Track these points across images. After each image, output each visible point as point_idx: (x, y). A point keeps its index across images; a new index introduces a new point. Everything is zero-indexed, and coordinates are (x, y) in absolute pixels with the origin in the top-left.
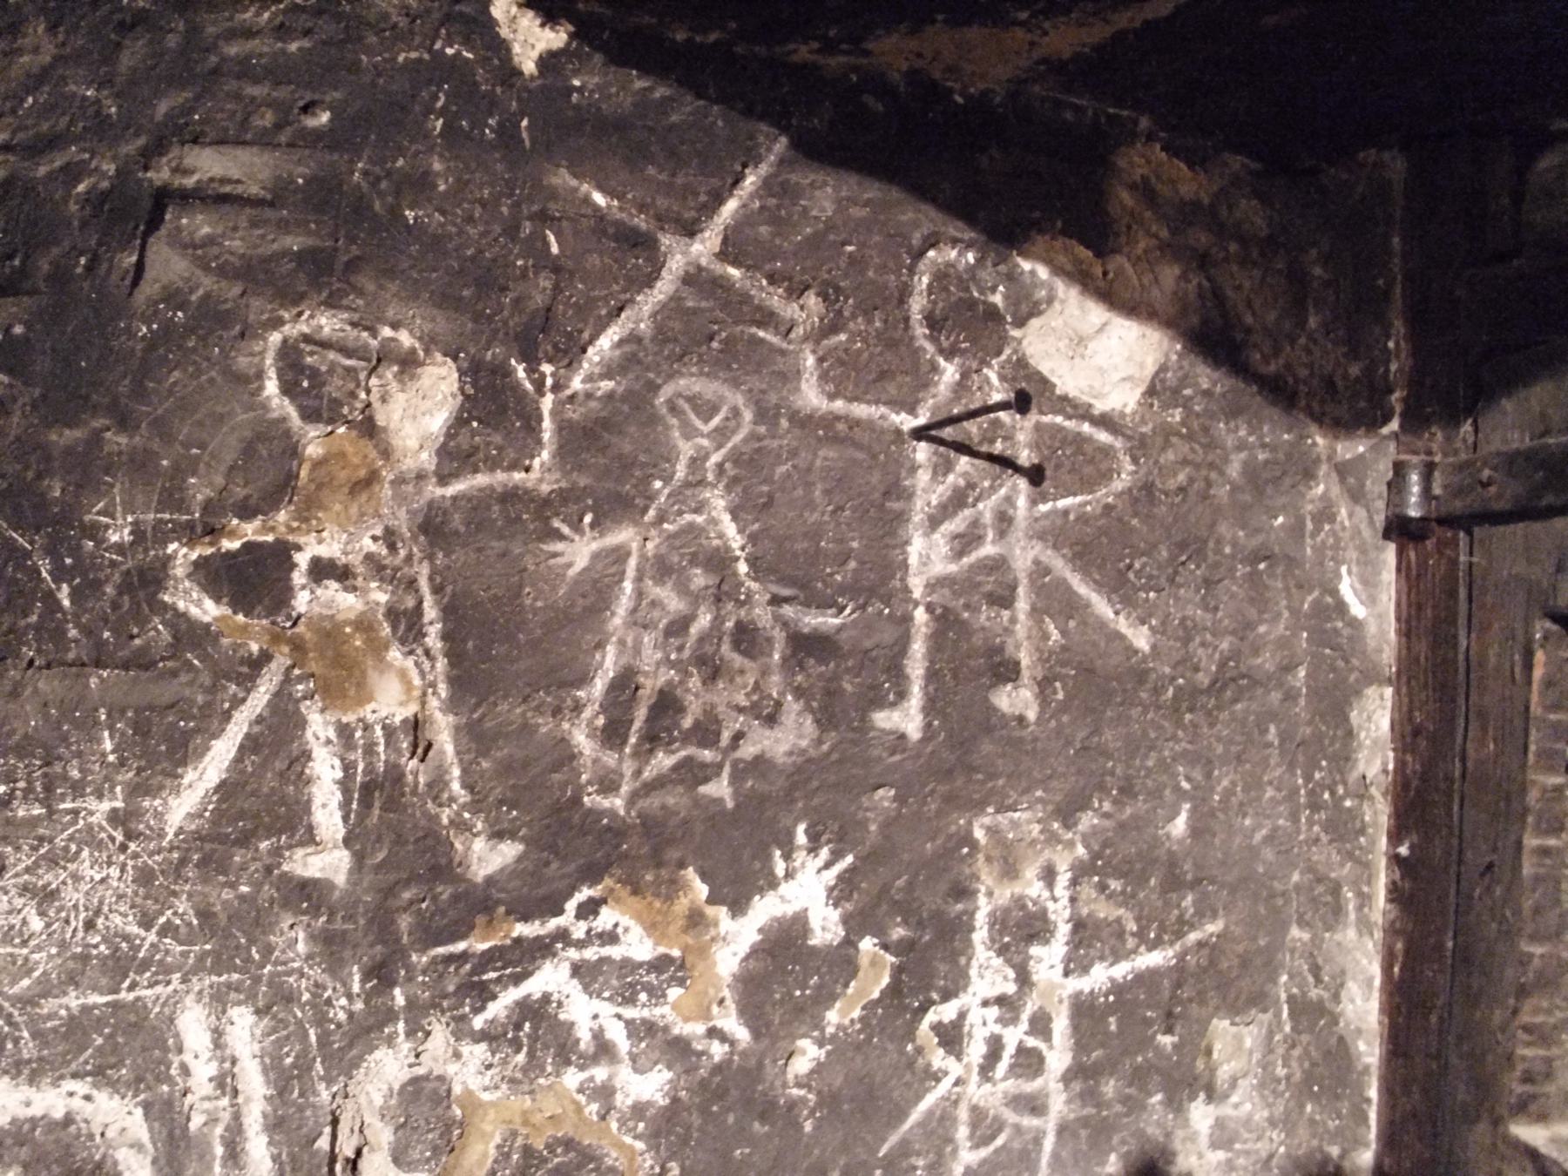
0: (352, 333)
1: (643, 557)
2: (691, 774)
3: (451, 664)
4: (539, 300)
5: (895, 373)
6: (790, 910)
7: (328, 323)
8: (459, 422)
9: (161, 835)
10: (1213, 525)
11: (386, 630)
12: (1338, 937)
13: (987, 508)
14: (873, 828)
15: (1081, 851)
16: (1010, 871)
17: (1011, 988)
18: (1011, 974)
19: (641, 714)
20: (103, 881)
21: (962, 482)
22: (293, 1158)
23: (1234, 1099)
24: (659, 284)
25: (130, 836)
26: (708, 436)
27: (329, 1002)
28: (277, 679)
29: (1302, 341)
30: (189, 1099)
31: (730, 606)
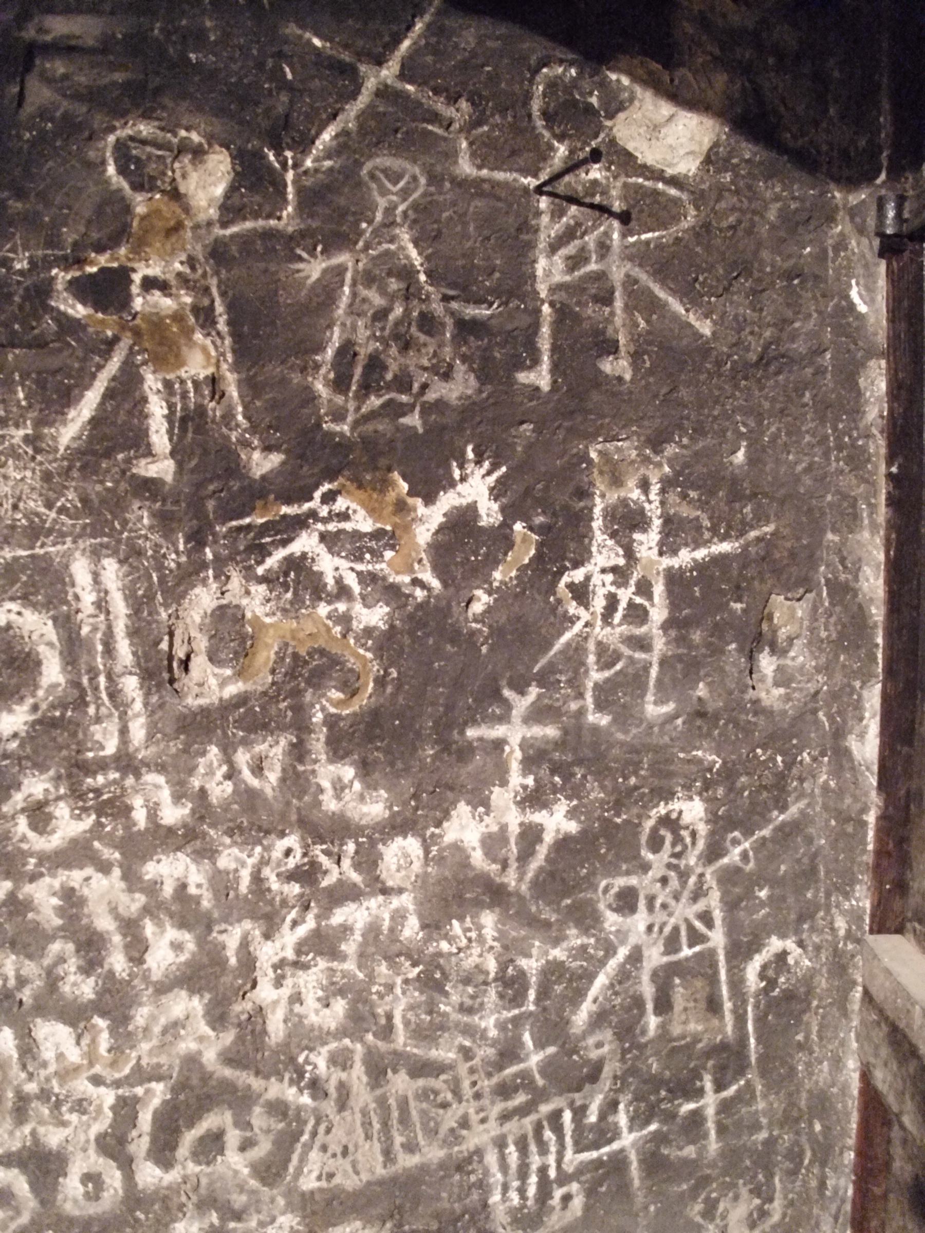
0: (160, 134)
1: (356, 271)
2: (394, 410)
3: (234, 342)
4: (280, 110)
5: (521, 148)
6: (464, 502)
7: (145, 129)
8: (232, 189)
9: (56, 450)
10: (756, 253)
11: (192, 320)
12: (858, 537)
13: (590, 240)
14: (519, 449)
15: (667, 469)
16: (617, 481)
17: (621, 562)
18: (621, 552)
19: (358, 371)
20: (22, 479)
21: (572, 222)
22: (145, 654)
23: (792, 654)
24: (360, 98)
25: (38, 451)
26: (396, 194)
27: (164, 556)
28: (124, 353)
29: (824, 125)
30: (80, 616)
31: (415, 302)
